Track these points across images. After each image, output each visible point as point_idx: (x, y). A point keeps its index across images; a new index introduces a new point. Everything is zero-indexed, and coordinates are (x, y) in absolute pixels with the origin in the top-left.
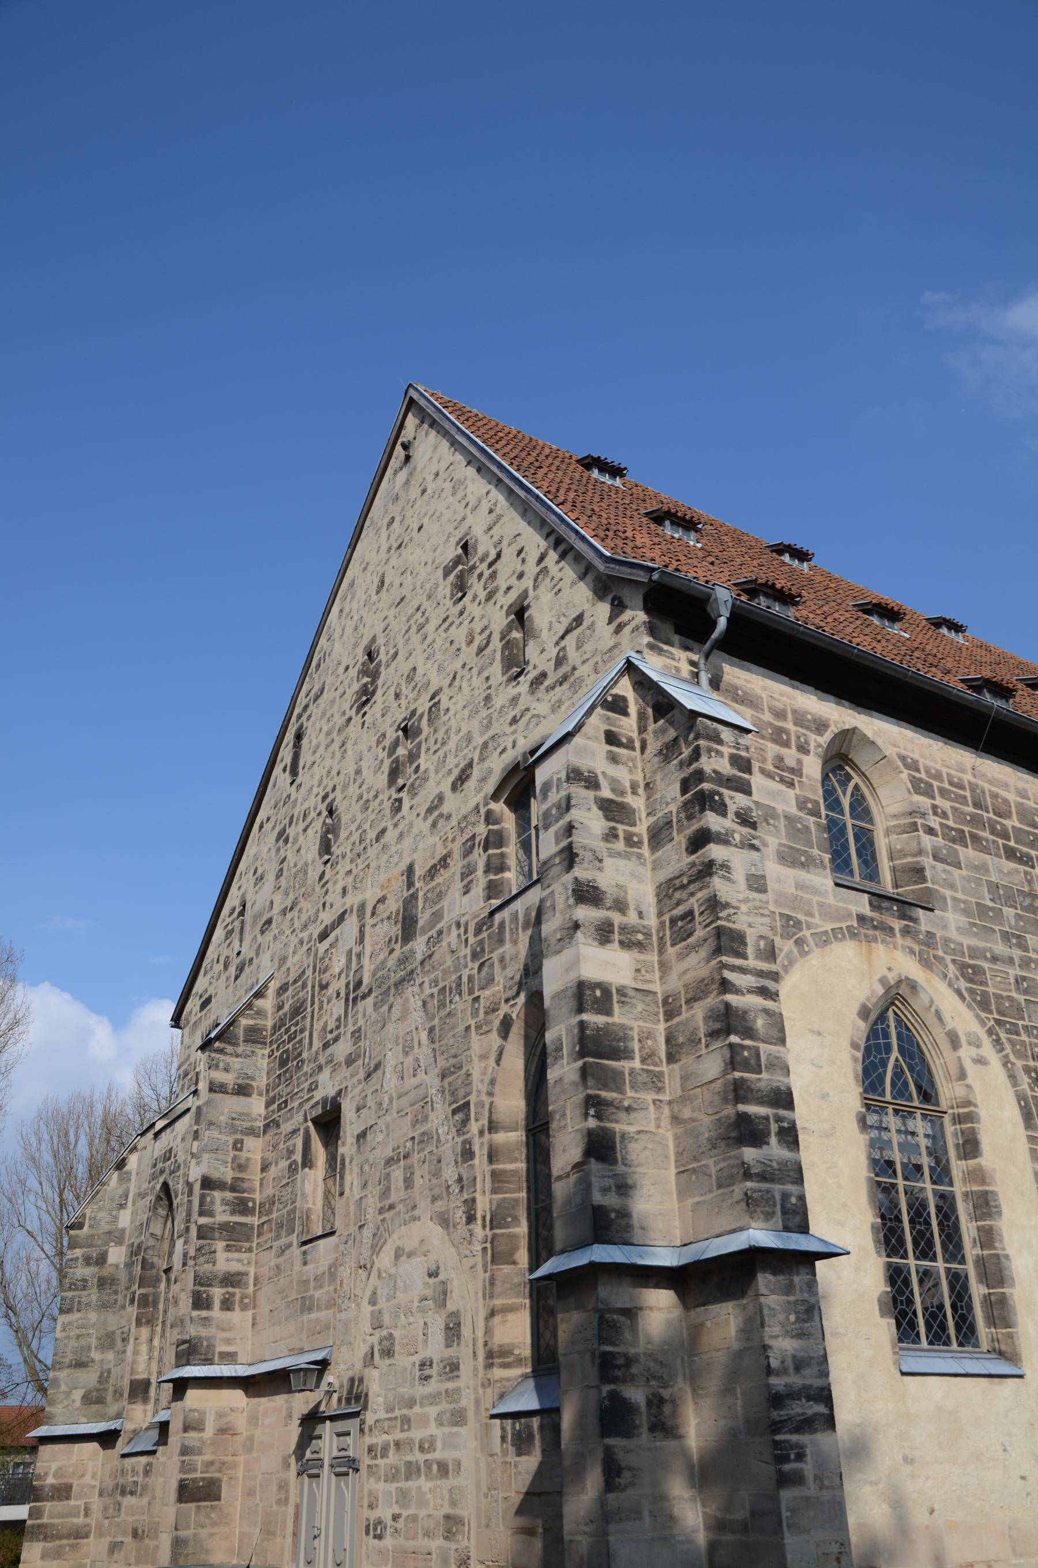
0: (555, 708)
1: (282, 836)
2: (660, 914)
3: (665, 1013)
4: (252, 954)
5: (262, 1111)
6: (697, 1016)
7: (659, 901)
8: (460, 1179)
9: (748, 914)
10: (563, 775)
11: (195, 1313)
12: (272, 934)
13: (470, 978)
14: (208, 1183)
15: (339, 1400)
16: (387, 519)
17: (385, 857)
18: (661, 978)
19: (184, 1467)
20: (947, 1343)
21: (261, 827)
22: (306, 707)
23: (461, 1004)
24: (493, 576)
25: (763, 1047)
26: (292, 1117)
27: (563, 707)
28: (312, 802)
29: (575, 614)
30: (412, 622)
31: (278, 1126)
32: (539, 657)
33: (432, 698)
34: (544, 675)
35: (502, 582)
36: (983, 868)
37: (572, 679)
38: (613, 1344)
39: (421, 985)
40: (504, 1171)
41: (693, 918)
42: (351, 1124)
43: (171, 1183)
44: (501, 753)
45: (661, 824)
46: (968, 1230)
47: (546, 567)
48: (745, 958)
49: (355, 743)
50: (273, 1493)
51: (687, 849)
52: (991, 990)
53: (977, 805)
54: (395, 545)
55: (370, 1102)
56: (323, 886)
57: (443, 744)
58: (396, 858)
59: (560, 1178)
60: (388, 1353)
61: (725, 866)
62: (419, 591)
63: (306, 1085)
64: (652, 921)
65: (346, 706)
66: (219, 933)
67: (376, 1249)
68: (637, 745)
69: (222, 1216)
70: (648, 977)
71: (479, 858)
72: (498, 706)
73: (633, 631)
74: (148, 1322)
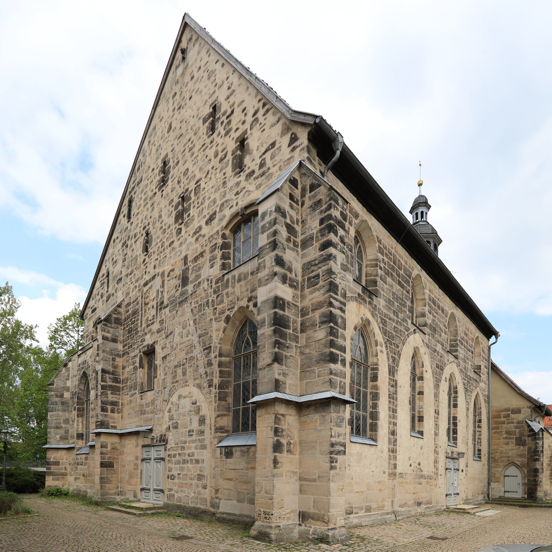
0: (258, 187)
1: (125, 245)
2: (303, 276)
3: (301, 314)
4: (114, 292)
5: (122, 349)
6: (317, 315)
7: (303, 271)
8: (206, 373)
9: (340, 279)
10: (273, 209)
11: (102, 413)
12: (122, 284)
13: (213, 301)
14: (103, 371)
15: (157, 441)
16: (173, 93)
17: (174, 253)
18: (301, 301)
19: (101, 458)
20: (360, 435)
21: (114, 241)
22: (133, 188)
23: (209, 311)
24: (229, 123)
25: (340, 330)
26: (134, 351)
27: (262, 187)
28: (138, 230)
29: (271, 141)
30: (186, 146)
31: (129, 354)
32: (251, 162)
33: (196, 183)
34: (253, 172)
35: (233, 126)
36: (391, 286)
37: (267, 174)
38: (278, 425)
39: (191, 303)
40: (224, 371)
41: (319, 277)
42: (159, 353)
43: (87, 372)
44: (230, 208)
45: (308, 238)
46: (370, 403)
47: (257, 118)
48: (338, 295)
49: (158, 204)
50: (132, 466)
51: (319, 249)
52: (388, 329)
53: (394, 263)
54: (177, 108)
55: (168, 345)
56: (145, 265)
57: (202, 204)
58: (179, 253)
59: (261, 369)
60: (176, 427)
61: (335, 257)
62: (190, 131)
63: (140, 340)
64: (300, 279)
65: (154, 187)
66: (98, 284)
67: (170, 395)
68: (300, 203)
69: (109, 383)
70: (296, 300)
71: (218, 253)
72: (229, 186)
73: (301, 150)
74: (81, 416)
